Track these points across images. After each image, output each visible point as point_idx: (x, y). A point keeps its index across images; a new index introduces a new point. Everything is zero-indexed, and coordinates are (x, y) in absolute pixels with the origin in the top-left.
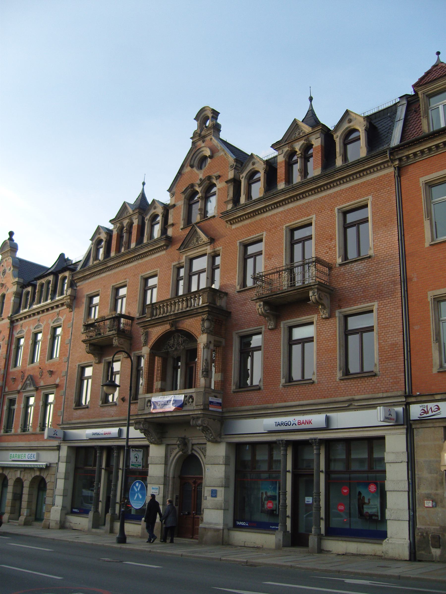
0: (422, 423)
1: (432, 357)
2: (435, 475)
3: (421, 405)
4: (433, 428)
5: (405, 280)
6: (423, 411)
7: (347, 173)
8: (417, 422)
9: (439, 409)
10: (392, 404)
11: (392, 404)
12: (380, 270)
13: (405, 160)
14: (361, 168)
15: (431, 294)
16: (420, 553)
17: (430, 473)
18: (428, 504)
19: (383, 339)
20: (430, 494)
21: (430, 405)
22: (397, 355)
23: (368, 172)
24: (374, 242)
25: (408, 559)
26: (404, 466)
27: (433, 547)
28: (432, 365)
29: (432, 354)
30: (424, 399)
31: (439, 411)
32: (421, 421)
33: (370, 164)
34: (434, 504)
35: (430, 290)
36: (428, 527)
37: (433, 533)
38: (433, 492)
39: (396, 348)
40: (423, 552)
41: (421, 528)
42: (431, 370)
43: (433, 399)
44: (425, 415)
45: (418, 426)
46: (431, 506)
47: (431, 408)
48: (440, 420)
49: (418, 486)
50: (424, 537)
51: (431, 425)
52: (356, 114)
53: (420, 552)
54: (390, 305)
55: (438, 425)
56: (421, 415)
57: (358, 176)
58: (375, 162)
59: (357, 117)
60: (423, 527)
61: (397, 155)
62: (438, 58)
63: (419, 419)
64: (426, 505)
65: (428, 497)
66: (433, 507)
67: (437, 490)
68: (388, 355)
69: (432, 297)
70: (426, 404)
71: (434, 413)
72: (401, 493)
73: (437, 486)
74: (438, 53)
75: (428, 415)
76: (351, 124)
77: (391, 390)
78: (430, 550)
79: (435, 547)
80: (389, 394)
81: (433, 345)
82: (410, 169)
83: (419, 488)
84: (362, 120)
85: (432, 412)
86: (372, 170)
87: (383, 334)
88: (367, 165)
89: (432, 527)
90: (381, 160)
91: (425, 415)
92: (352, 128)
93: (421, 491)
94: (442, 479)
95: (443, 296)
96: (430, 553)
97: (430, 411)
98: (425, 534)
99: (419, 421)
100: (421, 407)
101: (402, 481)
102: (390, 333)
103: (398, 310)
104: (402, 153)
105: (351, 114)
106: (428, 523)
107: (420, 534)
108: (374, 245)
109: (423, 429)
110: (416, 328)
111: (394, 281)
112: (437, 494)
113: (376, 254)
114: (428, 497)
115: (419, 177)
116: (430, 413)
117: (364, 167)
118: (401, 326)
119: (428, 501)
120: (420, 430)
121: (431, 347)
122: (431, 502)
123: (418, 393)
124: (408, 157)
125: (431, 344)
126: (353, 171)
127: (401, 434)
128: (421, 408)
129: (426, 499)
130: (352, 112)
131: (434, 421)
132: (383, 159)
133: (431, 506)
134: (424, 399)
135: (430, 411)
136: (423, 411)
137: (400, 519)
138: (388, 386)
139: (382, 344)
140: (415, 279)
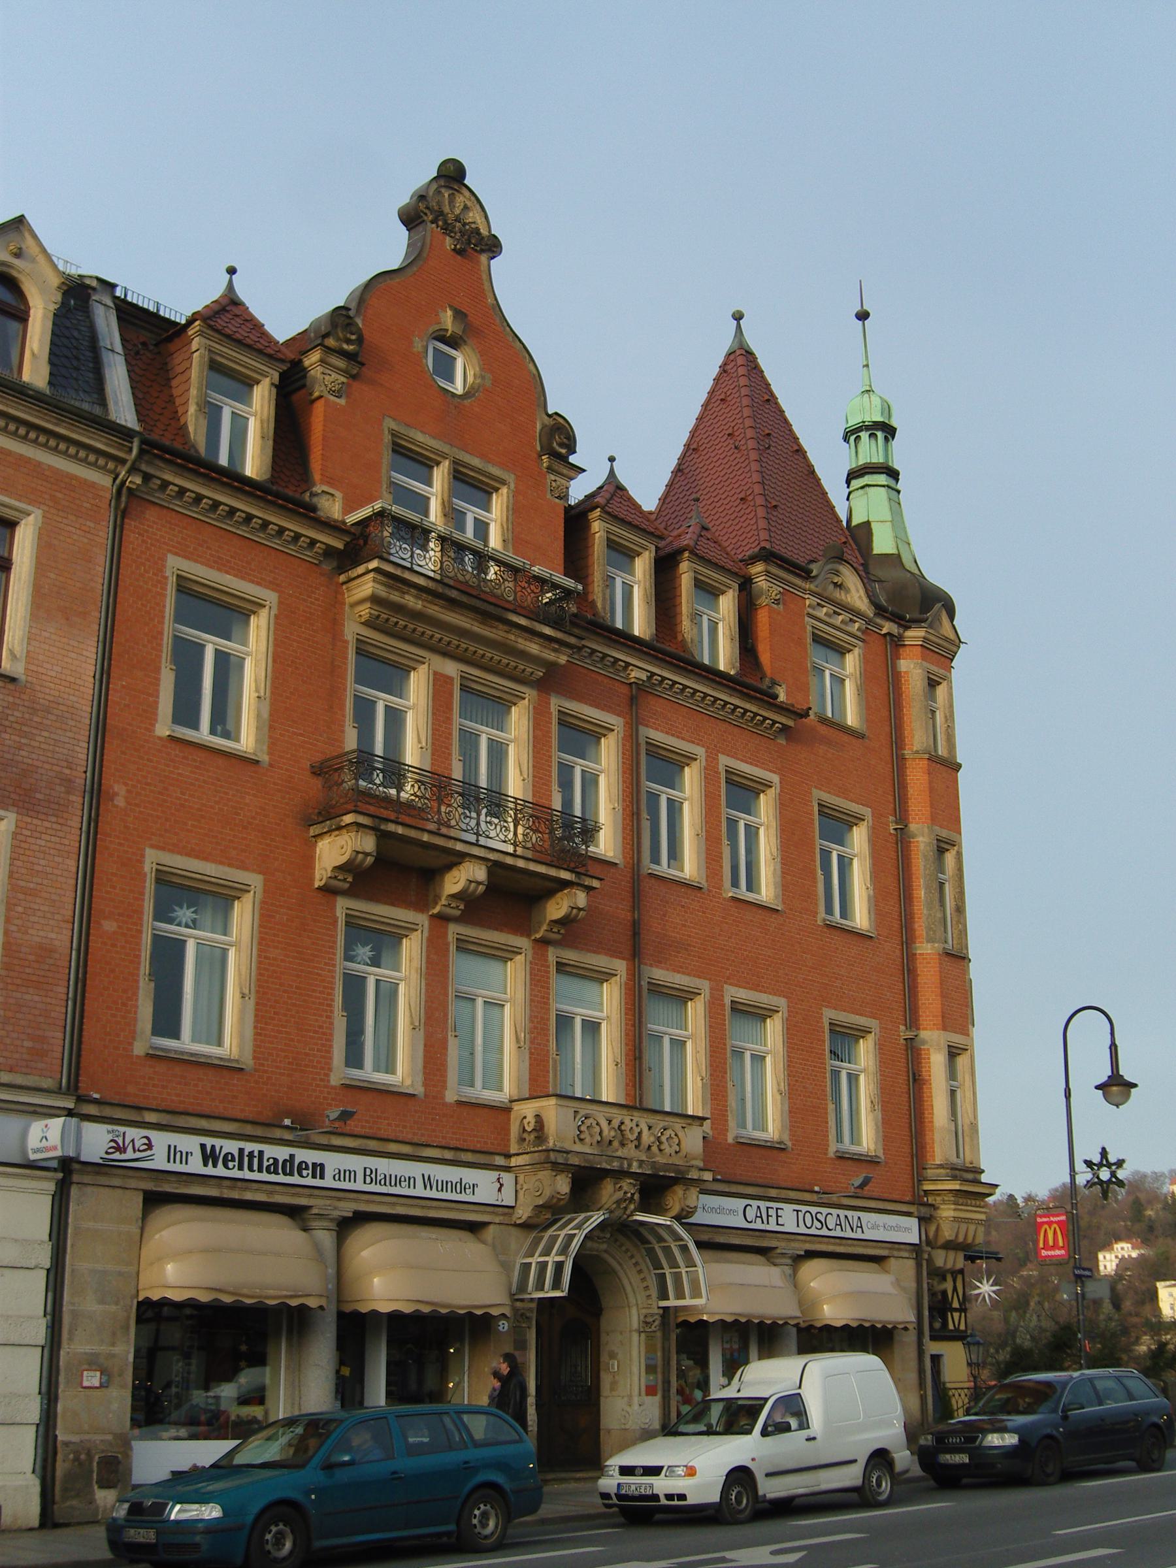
0: (98, 1173)
1: (136, 1013)
2: (113, 1308)
3: (110, 1127)
4: (120, 1191)
5: (97, 793)
6: (113, 1144)
7: (7, 405)
8: (89, 1169)
9: (150, 1146)
10: (32, 1109)
11: (32, 1109)
12: (34, 731)
13: (156, 487)
14: (48, 421)
15: (152, 858)
16: (60, 1509)
17: (102, 1302)
18: (92, 1379)
19: (19, 922)
20: (96, 1355)
21: (132, 1133)
22: (51, 981)
23: (52, 443)
24: (29, 644)
25: (35, 1522)
26: (39, 1280)
27: (101, 1487)
28: (134, 1032)
29: (137, 1007)
30: (118, 1114)
31: (149, 1153)
32: (101, 1168)
33: (73, 431)
34: (105, 1378)
35: (152, 846)
36: (87, 1437)
37: (103, 1451)
38: (104, 1349)
39: (51, 961)
40: (74, 1502)
41: (70, 1442)
42: (131, 1044)
43: (139, 1119)
44: (117, 1156)
45: (87, 1179)
46: (97, 1384)
47: (133, 1141)
48: (143, 1174)
49: (70, 1332)
50: (81, 1464)
51: (116, 1182)
52: (44, 251)
53: (68, 1503)
54: (48, 837)
55: (133, 1183)
56: (107, 1153)
57: (22, 431)
58: (90, 438)
59: (41, 259)
60: (75, 1438)
61: (149, 463)
62: (230, 282)
63: (101, 1161)
64: (86, 1384)
65: (93, 1362)
66: (101, 1386)
67: (113, 1344)
68: (27, 970)
69: (155, 867)
70: (122, 1129)
71: (138, 1155)
72: (24, 1350)
73: (114, 1334)
74: (232, 271)
75: (123, 1157)
76: (16, 262)
77: (24, 1070)
78: (92, 1493)
79: (102, 1486)
80: (19, 1080)
81: (141, 984)
82: (151, 514)
83: (70, 1339)
84: (55, 281)
85: (134, 1151)
86: (32, 435)
87: (20, 909)
88: (65, 428)
89: (98, 1438)
90: (107, 445)
91: (117, 1156)
92: (15, 273)
93: (73, 1348)
94: (128, 1318)
95: (176, 874)
96: (92, 1501)
97: (130, 1149)
98: (83, 1457)
99: (97, 1169)
100: (109, 1132)
101: (31, 1317)
102: (39, 913)
103: (68, 861)
104: (161, 469)
105: (27, 235)
106: (86, 1427)
107: (71, 1456)
108: (28, 652)
109: (95, 1189)
110: (109, 926)
111: (70, 781)
112: (113, 1356)
113: (30, 679)
114: (93, 1362)
115: (169, 551)
116: (130, 1154)
117: (57, 425)
118: (71, 907)
119: (91, 1373)
120: (89, 1189)
121: (138, 988)
122: (98, 1374)
123: (96, 1096)
124: (165, 484)
125: (137, 981)
126: (37, 417)
127: (41, 1192)
128: (110, 1137)
129: (86, 1367)
130: (35, 237)
131: (131, 1173)
132: (110, 446)
133: (97, 1384)
134: (118, 1114)
135: (130, 1149)
136: (113, 1144)
137: (18, 1420)
138: (17, 1056)
139: (14, 935)
140: (120, 802)
